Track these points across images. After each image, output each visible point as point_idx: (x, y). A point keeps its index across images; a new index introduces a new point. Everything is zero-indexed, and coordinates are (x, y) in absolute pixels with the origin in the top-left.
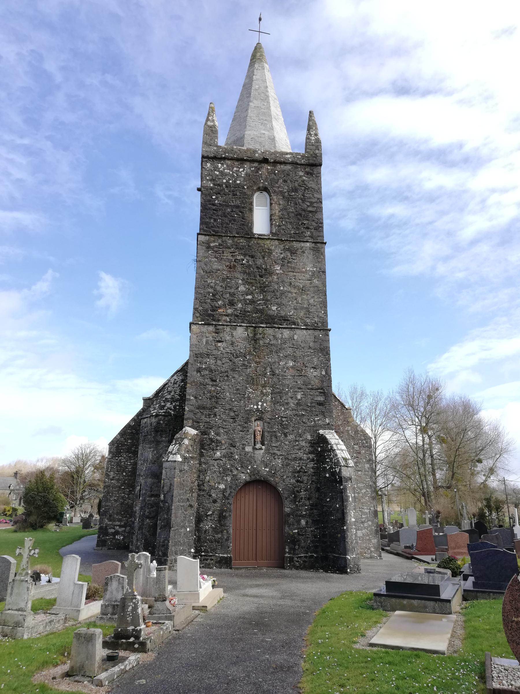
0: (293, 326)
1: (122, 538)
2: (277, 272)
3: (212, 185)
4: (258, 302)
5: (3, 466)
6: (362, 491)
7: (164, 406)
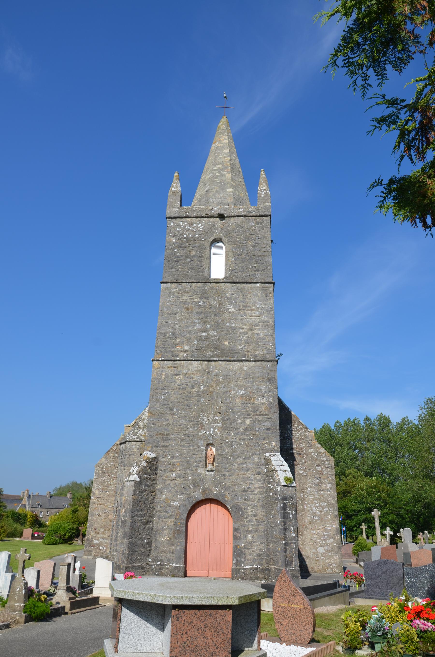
0: (244, 358)
1: (105, 548)
2: (230, 310)
3: (174, 240)
4: (212, 339)
5: (68, 484)
6: (325, 510)
7: (137, 433)
